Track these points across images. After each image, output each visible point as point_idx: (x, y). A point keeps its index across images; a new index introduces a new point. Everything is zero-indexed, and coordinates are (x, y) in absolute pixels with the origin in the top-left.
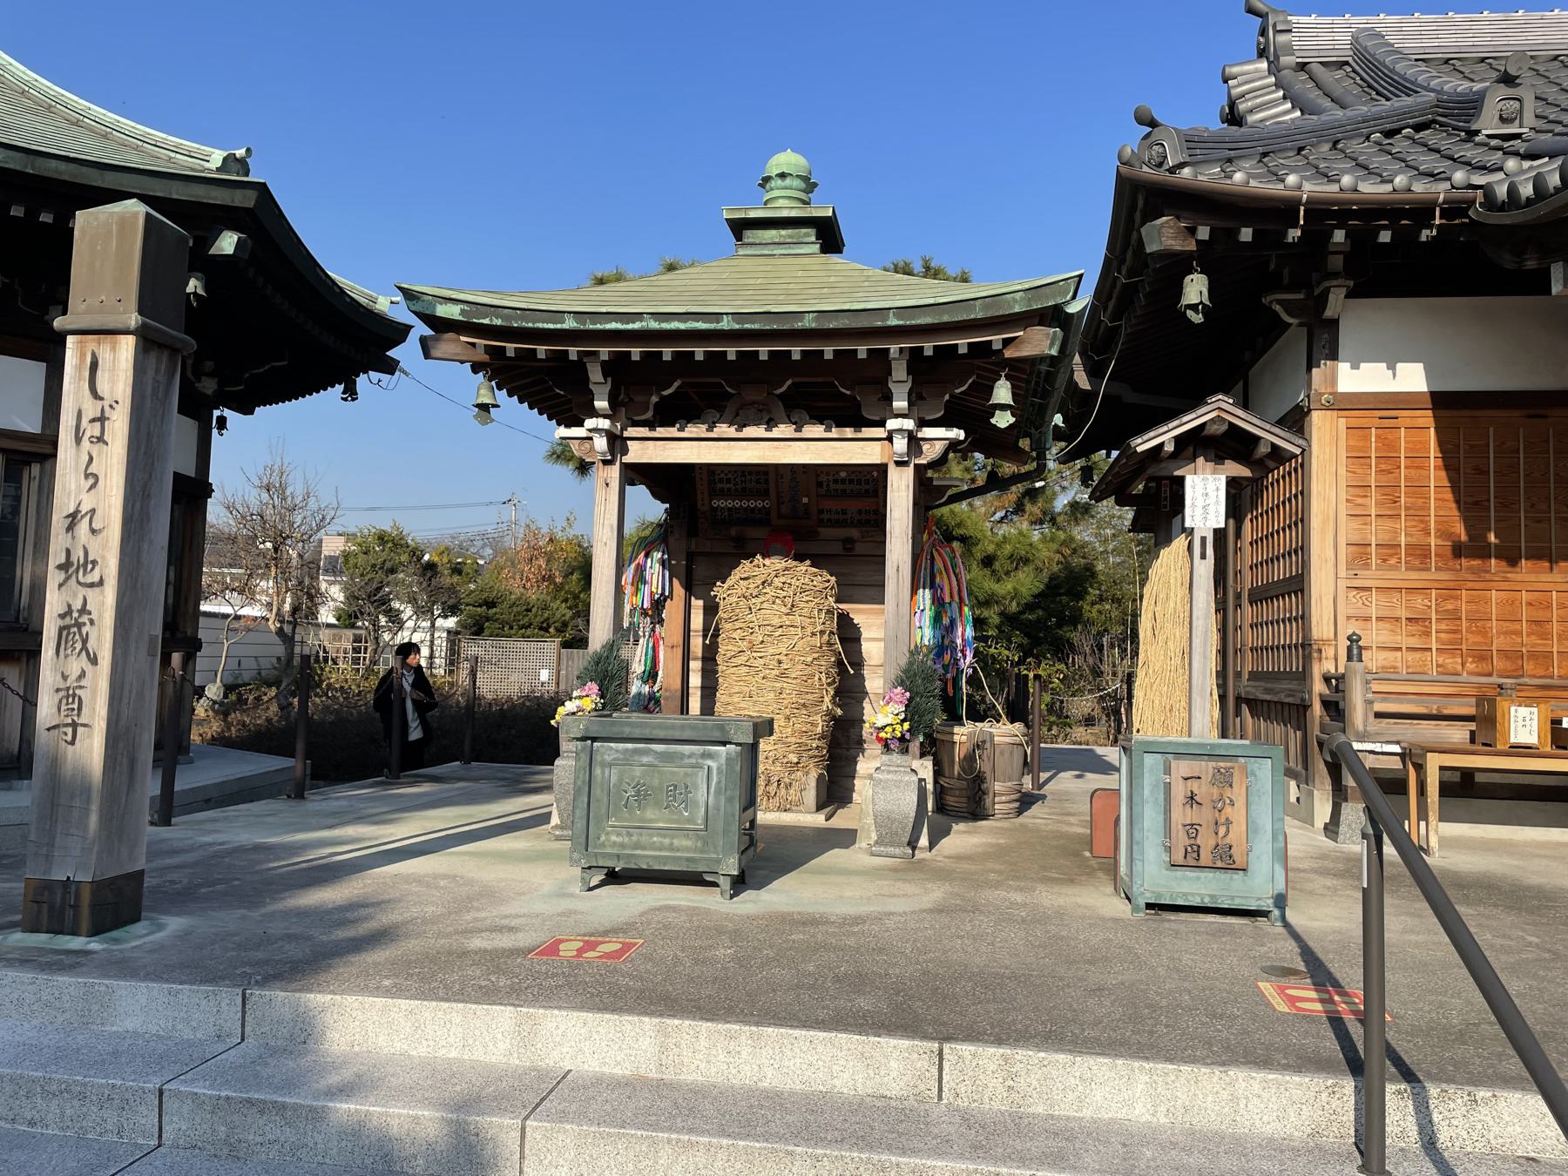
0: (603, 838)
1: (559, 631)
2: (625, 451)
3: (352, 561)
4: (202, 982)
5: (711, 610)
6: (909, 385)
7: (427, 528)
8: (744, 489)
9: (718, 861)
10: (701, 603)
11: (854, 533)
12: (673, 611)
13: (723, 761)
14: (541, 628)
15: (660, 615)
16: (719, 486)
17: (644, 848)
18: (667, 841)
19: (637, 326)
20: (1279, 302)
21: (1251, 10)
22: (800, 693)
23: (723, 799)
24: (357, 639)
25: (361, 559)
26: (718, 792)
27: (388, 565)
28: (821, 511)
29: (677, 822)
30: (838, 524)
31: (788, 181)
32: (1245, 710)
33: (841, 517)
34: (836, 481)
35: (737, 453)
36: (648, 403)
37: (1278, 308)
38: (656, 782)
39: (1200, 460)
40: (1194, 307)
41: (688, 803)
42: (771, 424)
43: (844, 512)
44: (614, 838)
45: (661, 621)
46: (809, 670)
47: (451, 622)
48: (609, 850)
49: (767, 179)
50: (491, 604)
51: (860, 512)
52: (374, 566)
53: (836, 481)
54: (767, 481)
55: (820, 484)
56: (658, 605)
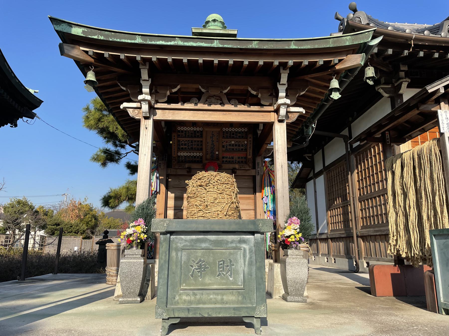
0: (177, 298)
1: (82, 234)
2: (155, 114)
3: (7, 210)
5: (179, 199)
6: (286, 86)
7: (37, 203)
8: (192, 148)
9: (254, 309)
11: (237, 166)
13: (252, 244)
14: (75, 233)
16: (182, 147)
17: (204, 303)
18: (219, 297)
19: (172, 43)
20: (382, 88)
21: (337, 19)
23: (254, 268)
24: (7, 238)
25: (10, 209)
26: (250, 264)
27: (21, 211)
28: (223, 158)
29: (226, 284)
30: (230, 162)
31: (216, 23)
32: (361, 241)
33: (231, 160)
34: (230, 145)
35: (206, 116)
36: (166, 94)
37: (381, 91)
38: (211, 259)
39: (442, 104)
40: (369, 78)
41: (235, 273)
42: (222, 104)
43: (232, 158)
44: (184, 297)
47: (42, 233)
48: (181, 306)
49: (208, 22)
50: (58, 225)
52: (15, 212)
53: (230, 145)
54: (202, 145)
55: (223, 147)
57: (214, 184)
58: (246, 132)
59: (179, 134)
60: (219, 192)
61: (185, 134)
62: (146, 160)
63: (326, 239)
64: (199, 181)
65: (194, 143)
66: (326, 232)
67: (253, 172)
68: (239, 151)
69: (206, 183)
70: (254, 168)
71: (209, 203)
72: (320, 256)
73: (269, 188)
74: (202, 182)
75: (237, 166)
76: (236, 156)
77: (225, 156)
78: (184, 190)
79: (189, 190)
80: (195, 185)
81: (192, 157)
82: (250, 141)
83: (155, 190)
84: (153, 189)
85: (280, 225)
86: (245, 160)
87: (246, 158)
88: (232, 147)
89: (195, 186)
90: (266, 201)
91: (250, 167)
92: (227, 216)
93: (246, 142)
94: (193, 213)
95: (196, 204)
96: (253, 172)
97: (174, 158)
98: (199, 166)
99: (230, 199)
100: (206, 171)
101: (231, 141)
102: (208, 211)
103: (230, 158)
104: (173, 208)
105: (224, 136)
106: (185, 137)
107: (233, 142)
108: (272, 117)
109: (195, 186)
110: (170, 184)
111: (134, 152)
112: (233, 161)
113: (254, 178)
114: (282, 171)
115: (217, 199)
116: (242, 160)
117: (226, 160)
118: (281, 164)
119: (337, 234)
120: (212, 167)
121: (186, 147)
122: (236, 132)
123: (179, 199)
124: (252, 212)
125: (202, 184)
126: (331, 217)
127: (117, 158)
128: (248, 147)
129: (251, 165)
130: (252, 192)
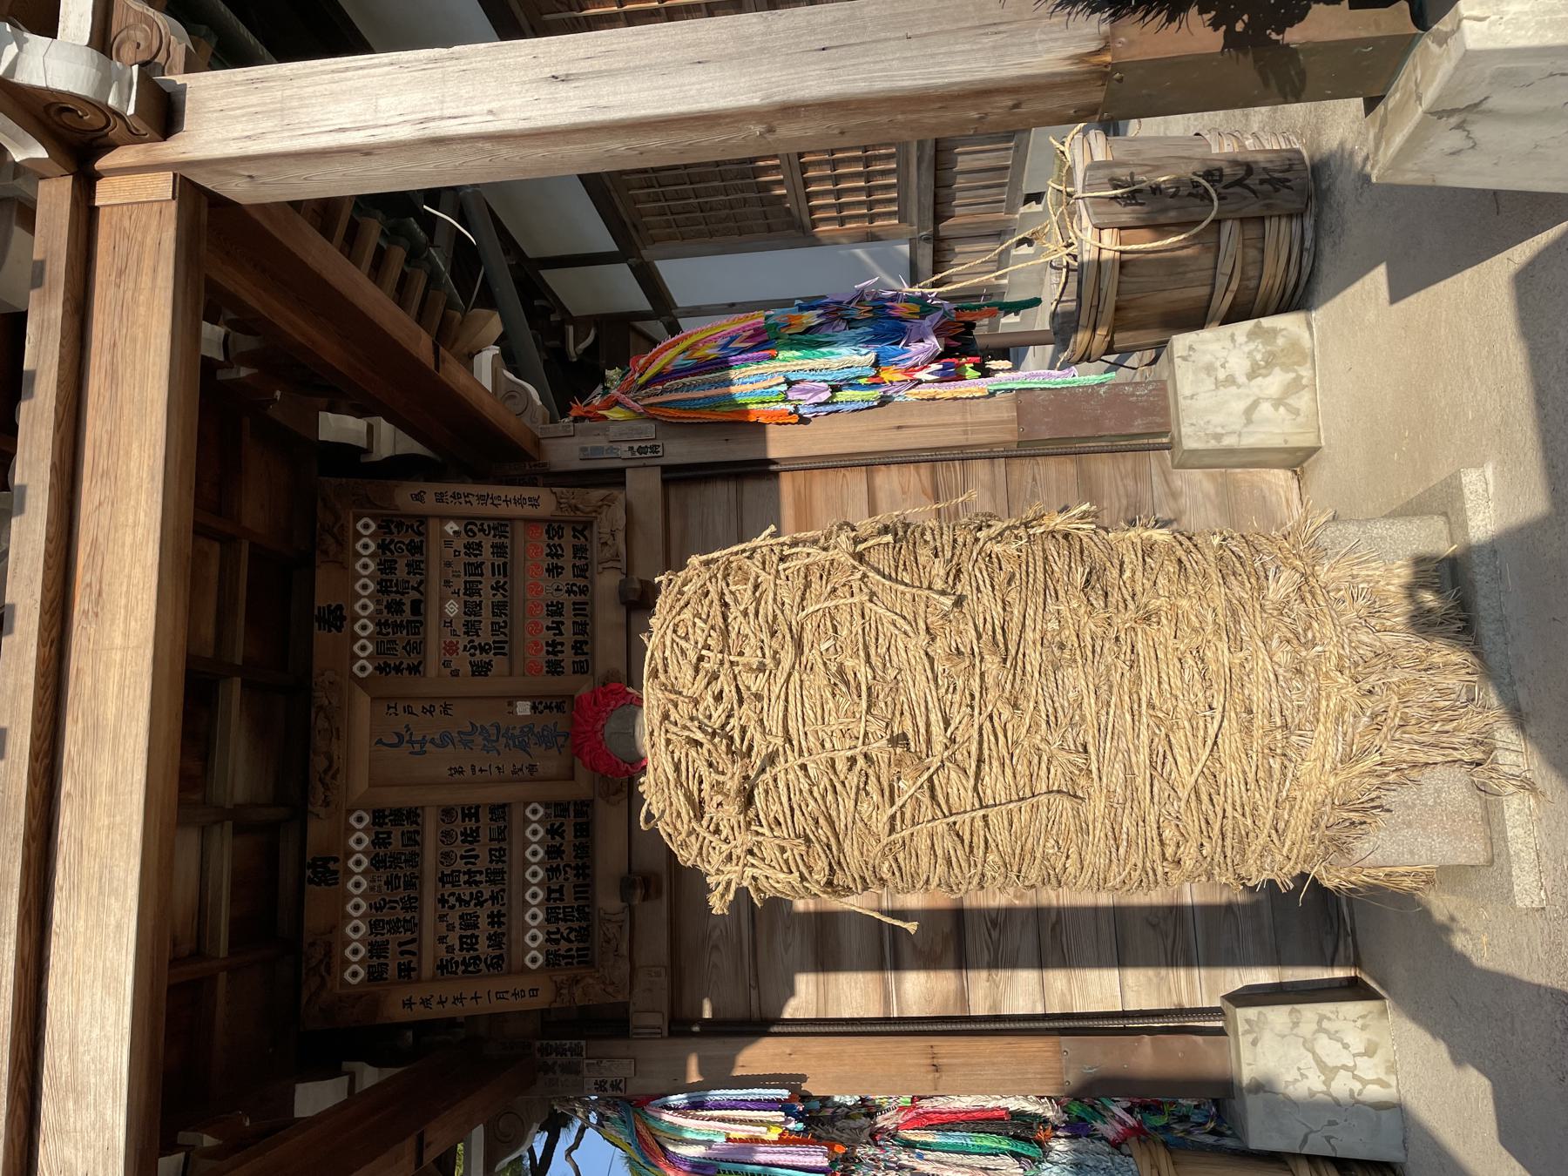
5: (829, 942)
10: (805, 984)
11: (607, 582)
12: (835, 1074)
15: (849, 1113)
16: (483, 947)
22: (1050, 591)
28: (554, 668)
33: (568, 619)
34: (471, 628)
35: (104, 772)
43: (555, 609)
45: (868, 1109)
51: (554, 570)
53: (471, 628)
54: (471, 812)
55: (481, 670)
56: (816, 1118)
57: (730, 693)
58: (385, 525)
61: (394, 926)
63: (936, 251)
64: (710, 809)
65: (460, 865)
66: (906, 248)
67: (644, 486)
68: (504, 570)
69: (723, 761)
70: (616, 478)
71: (875, 727)
73: (734, 374)
74: (718, 787)
75: (607, 582)
76: (536, 585)
77: (543, 657)
79: (778, 881)
80: (744, 839)
81: (552, 871)
82: (440, 498)
83: (778, 1116)
84: (774, 1134)
85: (1080, 58)
86: (568, 533)
87: (553, 527)
89: (750, 839)
90: (817, 392)
91: (607, 502)
92: (963, 587)
93: (451, 527)
95: (880, 823)
98: (608, 819)
99: (838, 579)
100: (637, 766)
102: (937, 728)
104: (891, 976)
106: (414, 926)
107: (453, 608)
108: (136, 190)
109: (750, 839)
110: (737, 1010)
111: (576, 1146)
112: (579, 608)
113: (678, 477)
114: (599, 74)
115: (841, 671)
116: (569, 552)
118: (545, 91)
120: (612, 726)
121: (483, 914)
122: (383, 587)
123: (829, 942)
124: (889, 480)
125: (732, 785)
128: (477, 509)
129: (596, 494)
130: (764, 485)
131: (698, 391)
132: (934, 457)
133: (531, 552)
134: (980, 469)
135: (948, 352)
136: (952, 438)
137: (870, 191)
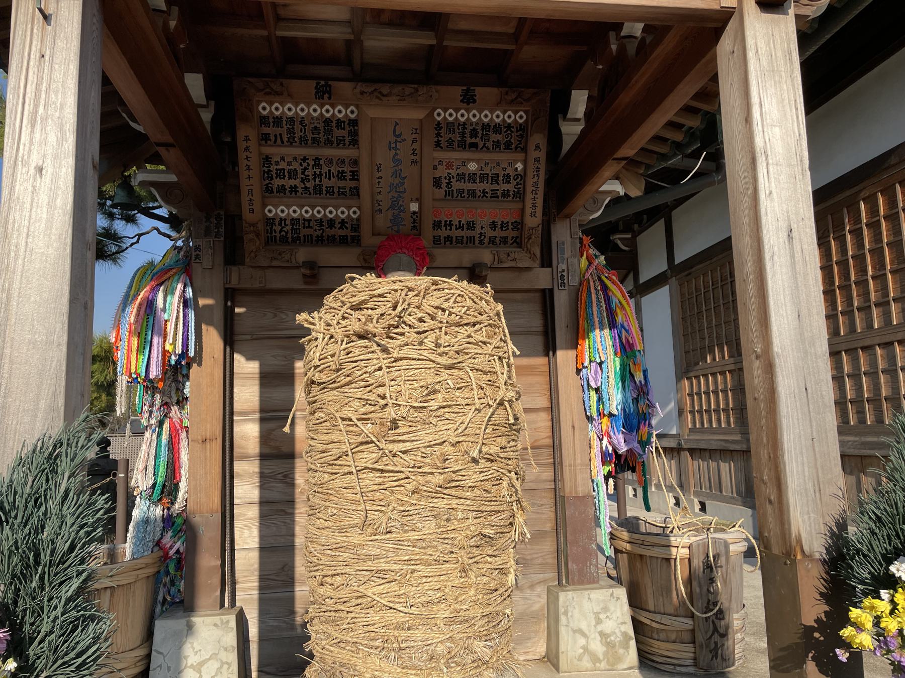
4: (235, 163)
5: (277, 379)
10: (253, 367)
11: (486, 256)
12: (202, 383)
15: (180, 390)
16: (277, 182)
28: (437, 225)
33: (466, 233)
43: (471, 226)
45: (182, 401)
46: (493, 469)
51: (493, 225)
53: (461, 177)
54: (355, 176)
55: (437, 183)
56: (177, 371)
57: (423, 327)
58: (522, 128)
59: (266, 130)
60: (443, 360)
61: (291, 131)
62: (44, 198)
64: (356, 314)
65: (325, 169)
66: (674, 432)
67: (542, 278)
68: (494, 196)
69: (385, 322)
70: (546, 261)
71: (403, 411)
72: (653, 489)
73: (607, 331)
74: (370, 319)
75: (486, 256)
76: (484, 215)
77: (443, 218)
78: (294, 342)
79: (314, 352)
80: (339, 333)
81: (320, 222)
82: (537, 160)
83: (179, 350)
84: (168, 347)
85: (799, 541)
86: (515, 234)
87: (519, 225)
88: (470, 186)
89: (339, 337)
90: (595, 379)
91: (533, 257)
92: (483, 463)
93: (520, 166)
94: (335, 452)
95: (348, 412)
96: (542, 278)
97: (253, 225)
98: (349, 255)
99: (489, 390)
101: (464, 164)
103: (460, 227)
104: (257, 416)
105: (438, 144)
106: (291, 142)
107: (473, 167)
109: (339, 337)
110: (239, 327)
112: (471, 240)
113: (546, 298)
115: (436, 391)
116: (504, 234)
117: (448, 233)
118: (783, 225)
119: (714, 441)
120: (405, 258)
121: (297, 182)
122: (486, 127)
123: (277, 379)
124: (543, 420)
125: (370, 327)
126: (691, 395)
127: (114, 249)
128: (530, 181)
129: (537, 251)
130: (540, 348)
131: (597, 310)
132: (555, 447)
133: (505, 212)
134: (548, 474)
135: (618, 456)
136: (567, 461)
137: (708, 411)
